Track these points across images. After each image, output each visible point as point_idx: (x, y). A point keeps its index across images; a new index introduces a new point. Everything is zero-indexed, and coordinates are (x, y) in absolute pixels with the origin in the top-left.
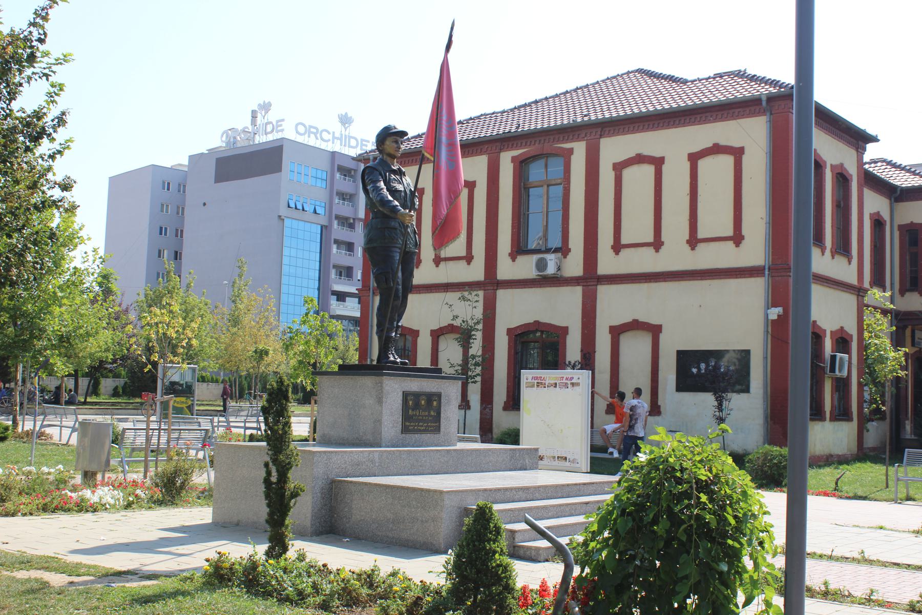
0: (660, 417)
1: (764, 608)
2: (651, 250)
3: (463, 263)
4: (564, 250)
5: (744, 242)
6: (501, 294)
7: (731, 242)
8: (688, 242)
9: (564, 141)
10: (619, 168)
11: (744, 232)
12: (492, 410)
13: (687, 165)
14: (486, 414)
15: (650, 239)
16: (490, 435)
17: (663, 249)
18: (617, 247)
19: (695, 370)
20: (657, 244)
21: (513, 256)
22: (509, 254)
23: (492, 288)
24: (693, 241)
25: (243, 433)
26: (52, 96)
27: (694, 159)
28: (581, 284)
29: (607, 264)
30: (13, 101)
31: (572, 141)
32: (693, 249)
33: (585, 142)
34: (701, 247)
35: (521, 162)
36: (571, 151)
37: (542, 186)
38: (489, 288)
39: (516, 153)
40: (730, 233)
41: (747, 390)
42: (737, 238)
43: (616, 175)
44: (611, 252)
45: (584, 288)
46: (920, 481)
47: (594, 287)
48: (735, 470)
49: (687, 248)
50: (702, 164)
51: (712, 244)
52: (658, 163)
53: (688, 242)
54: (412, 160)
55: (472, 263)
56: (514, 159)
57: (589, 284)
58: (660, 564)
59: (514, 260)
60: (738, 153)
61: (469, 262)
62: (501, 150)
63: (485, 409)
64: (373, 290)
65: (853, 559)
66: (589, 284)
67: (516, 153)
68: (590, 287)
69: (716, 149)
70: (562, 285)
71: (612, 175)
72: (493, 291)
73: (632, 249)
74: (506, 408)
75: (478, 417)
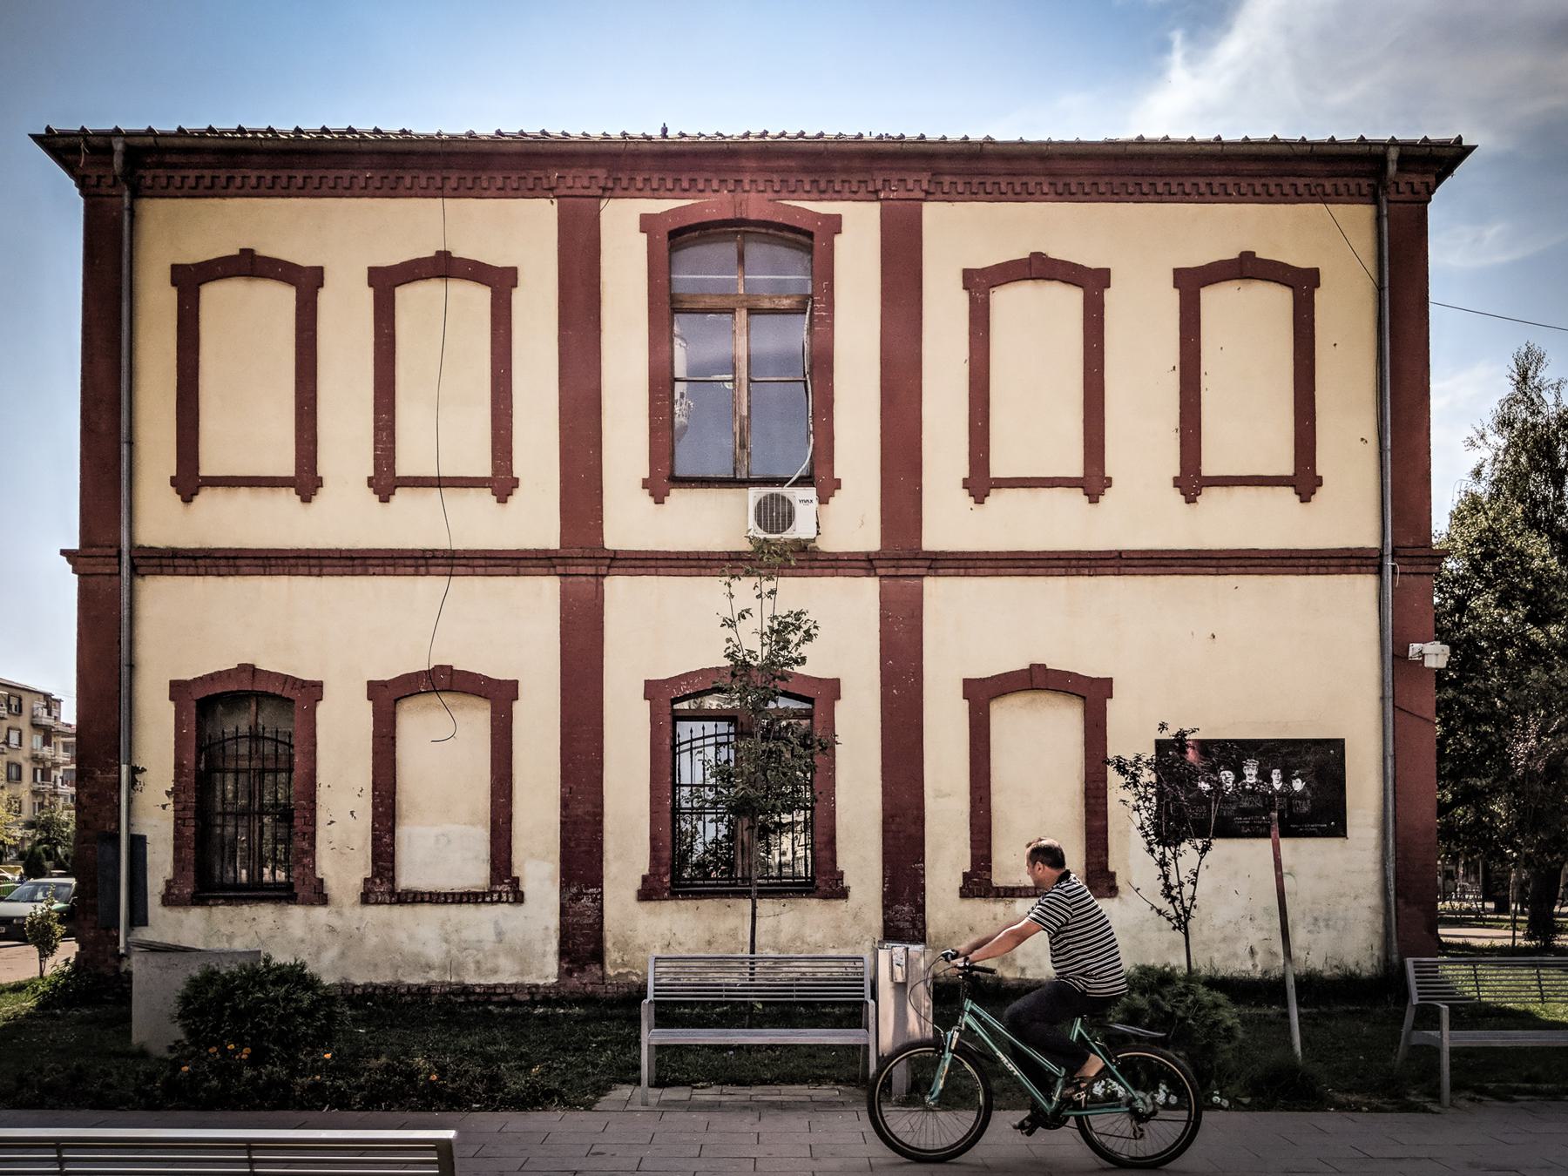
0: (1116, 900)
2: (1077, 496)
3: (289, 497)
4: (821, 479)
5: (518, 494)
6: (617, 588)
7: (1291, 490)
8: (1177, 482)
9: (822, 195)
10: (980, 283)
11: (323, 469)
12: (599, 899)
13: (1171, 299)
14: (582, 914)
16: (595, 969)
18: (980, 484)
19: (1298, 785)
20: (1093, 483)
22: (1176, 480)
23: (592, 570)
24: (385, 483)
27: (1191, 283)
28: (880, 571)
31: (838, 196)
32: (1190, 500)
33: (876, 206)
35: (674, 234)
36: (834, 224)
37: (732, 311)
38: (582, 570)
40: (288, 468)
41: (1337, 829)
42: (1305, 482)
43: (972, 300)
45: (885, 582)
46: (1565, 991)
47: (916, 581)
48: (522, 973)
49: (1176, 497)
51: (1240, 492)
53: (1177, 482)
54: (230, 179)
55: (513, 500)
56: (648, 223)
57: (902, 572)
59: (659, 500)
61: (503, 497)
62: (608, 192)
63: (577, 898)
64: (131, 558)
66: (902, 572)
68: (902, 581)
69: (1039, 268)
70: (817, 571)
72: (592, 579)
73: (1252, 490)
74: (648, 892)
75: (554, 921)
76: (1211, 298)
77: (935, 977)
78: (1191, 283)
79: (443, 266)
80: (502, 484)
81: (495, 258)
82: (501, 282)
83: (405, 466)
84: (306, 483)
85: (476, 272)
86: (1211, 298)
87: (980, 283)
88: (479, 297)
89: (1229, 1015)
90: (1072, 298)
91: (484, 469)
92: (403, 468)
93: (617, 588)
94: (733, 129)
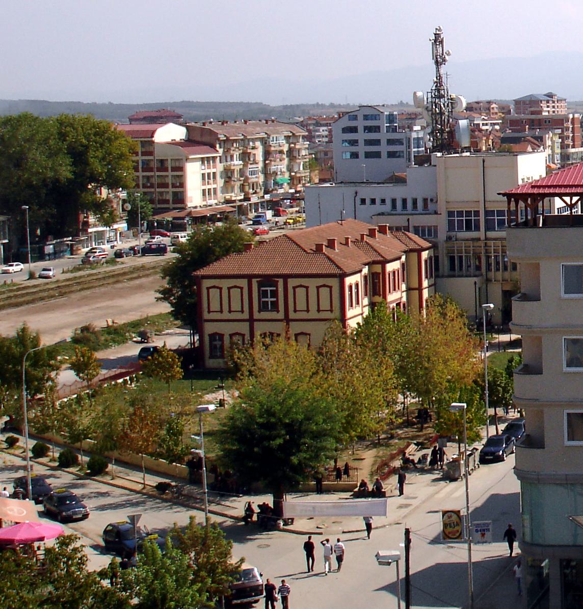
1: (213, 475)
6: (255, 323)
10: (294, 288)
15: (306, 309)
17: (310, 313)
18: (295, 311)
21: (260, 311)
24: (230, 311)
25: (427, 289)
26: (109, 163)
27: (318, 288)
29: (292, 315)
30: (443, 65)
34: (321, 312)
36: (278, 281)
39: (258, 279)
44: (293, 313)
50: (320, 289)
52: (307, 288)
56: (257, 281)
58: (26, 514)
60: (331, 287)
65: (90, 498)
67: (258, 279)
69: (324, 286)
71: (292, 290)
76: (297, 290)
77: (24, 330)
78: (318, 288)
79: (301, 286)
80: (242, 311)
81: (330, 285)
82: (242, 288)
83: (297, 309)
84: (221, 311)
85: (217, 287)
86: (320, 289)
87: (294, 288)
88: (218, 290)
89: (495, 438)
90: (328, 289)
91: (306, 309)
92: (321, 309)
93: (255, 323)
94: (417, 265)
